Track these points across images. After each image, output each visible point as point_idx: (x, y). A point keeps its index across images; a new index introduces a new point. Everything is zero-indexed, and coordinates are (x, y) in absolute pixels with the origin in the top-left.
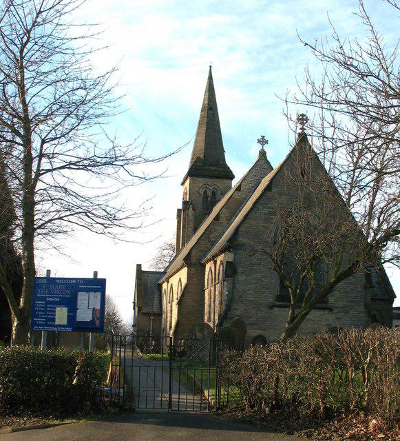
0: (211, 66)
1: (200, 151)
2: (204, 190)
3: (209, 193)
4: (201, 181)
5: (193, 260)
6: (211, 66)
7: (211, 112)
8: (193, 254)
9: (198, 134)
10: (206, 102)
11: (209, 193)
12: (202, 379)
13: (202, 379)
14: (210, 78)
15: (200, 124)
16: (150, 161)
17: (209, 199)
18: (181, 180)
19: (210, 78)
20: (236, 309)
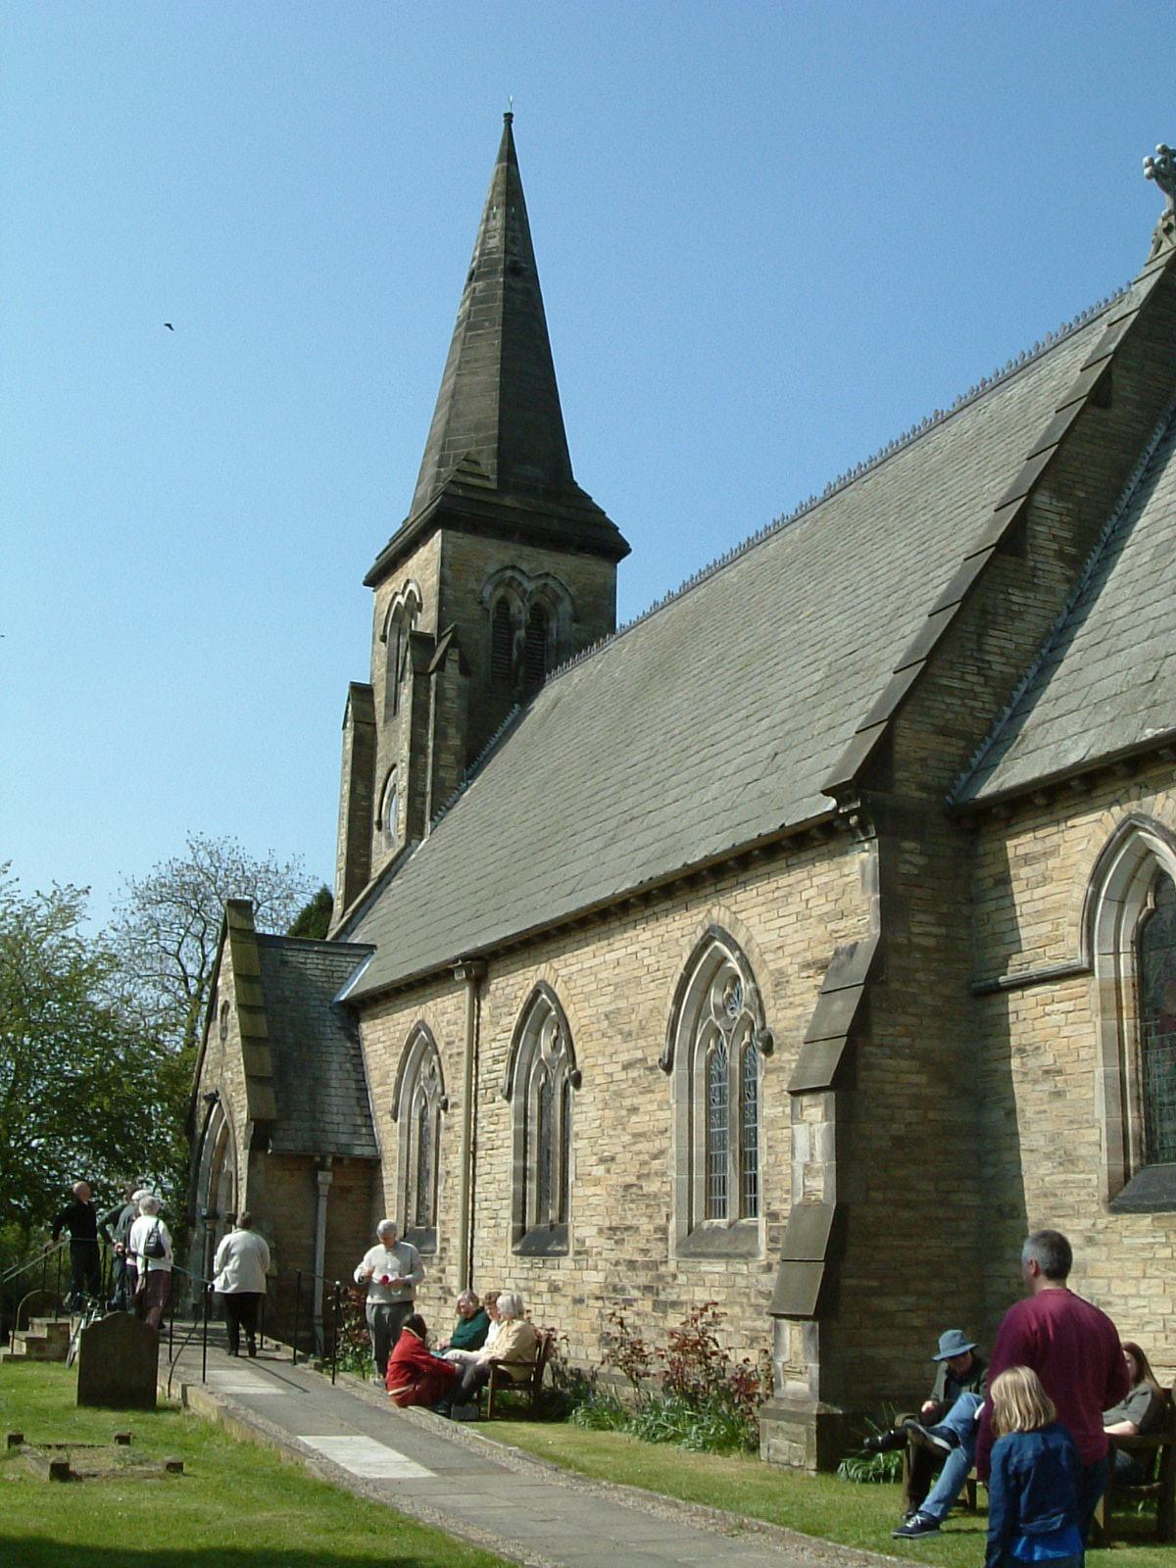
0: (509, 117)
1: (477, 428)
2: (501, 592)
3: (519, 609)
4: (494, 554)
5: (907, 788)
6: (509, 117)
7: (519, 284)
8: (904, 746)
9: (462, 364)
10: (495, 242)
11: (519, 609)
12: (205, 1346)
13: (205, 1346)
14: (509, 155)
15: (470, 325)
16: (965, 1532)
17: (521, 633)
18: (369, 564)
19: (509, 155)
20: (900, 745)
